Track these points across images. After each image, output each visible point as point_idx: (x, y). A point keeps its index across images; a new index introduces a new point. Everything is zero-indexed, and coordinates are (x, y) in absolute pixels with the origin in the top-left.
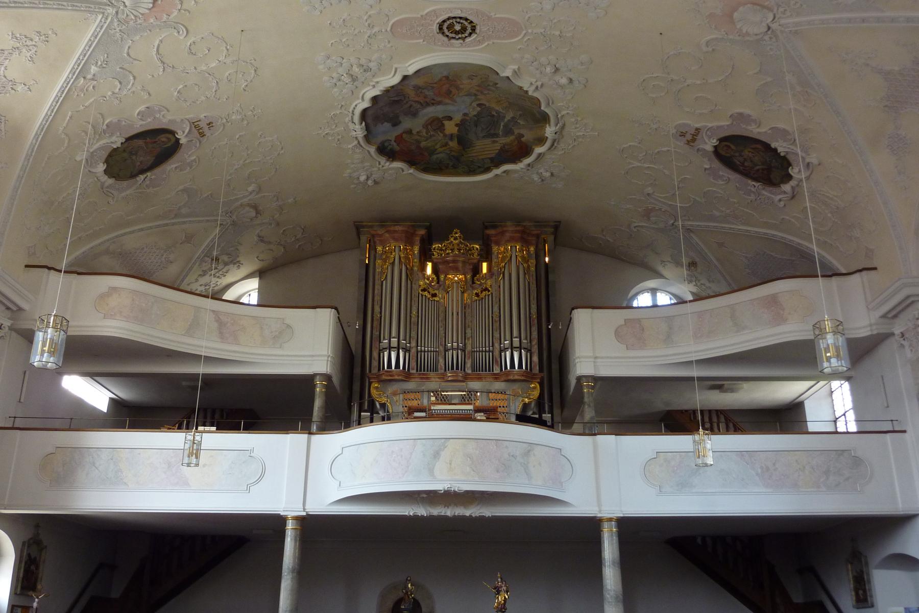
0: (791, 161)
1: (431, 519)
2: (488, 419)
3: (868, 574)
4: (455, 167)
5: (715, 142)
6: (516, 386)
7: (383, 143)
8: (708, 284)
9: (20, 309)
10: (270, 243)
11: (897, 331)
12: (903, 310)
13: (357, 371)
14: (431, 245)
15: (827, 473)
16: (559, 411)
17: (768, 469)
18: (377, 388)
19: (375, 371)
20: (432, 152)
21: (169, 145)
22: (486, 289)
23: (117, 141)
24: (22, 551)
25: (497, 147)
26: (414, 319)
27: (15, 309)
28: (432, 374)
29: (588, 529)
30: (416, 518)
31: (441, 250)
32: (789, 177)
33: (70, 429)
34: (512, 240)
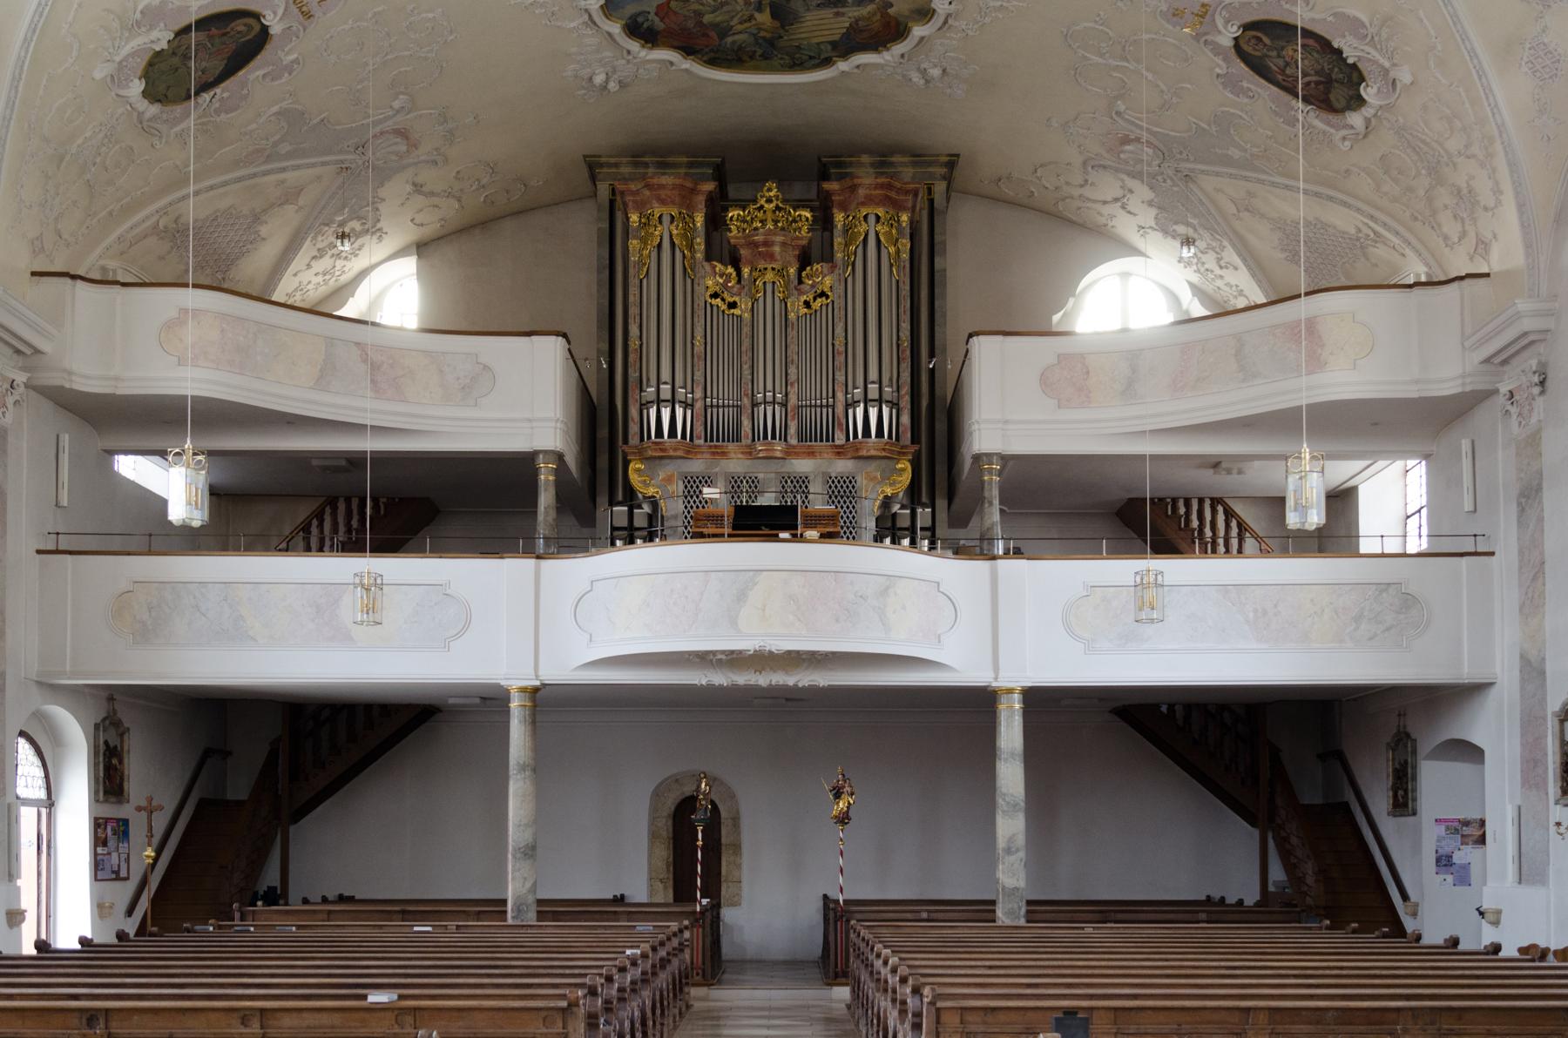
0: (1365, 74)
1: (735, 688)
2: (827, 537)
3: (1414, 767)
4: (765, 57)
5: (1234, 31)
6: (872, 467)
7: (633, 18)
8: (1218, 271)
9: (37, 351)
10: (432, 194)
11: (1504, 389)
12: (1517, 353)
13: (603, 433)
14: (726, 210)
15: (1358, 619)
16: (946, 502)
17: (1265, 612)
18: (639, 470)
19: (634, 440)
20: (724, 31)
21: (253, 34)
22: (823, 294)
23: (161, 38)
24: (96, 738)
25: (845, 23)
26: (699, 347)
27: (28, 351)
28: (731, 446)
29: (977, 705)
30: (711, 689)
31: (744, 221)
32: (1358, 102)
33: (150, 553)
34: (869, 201)
